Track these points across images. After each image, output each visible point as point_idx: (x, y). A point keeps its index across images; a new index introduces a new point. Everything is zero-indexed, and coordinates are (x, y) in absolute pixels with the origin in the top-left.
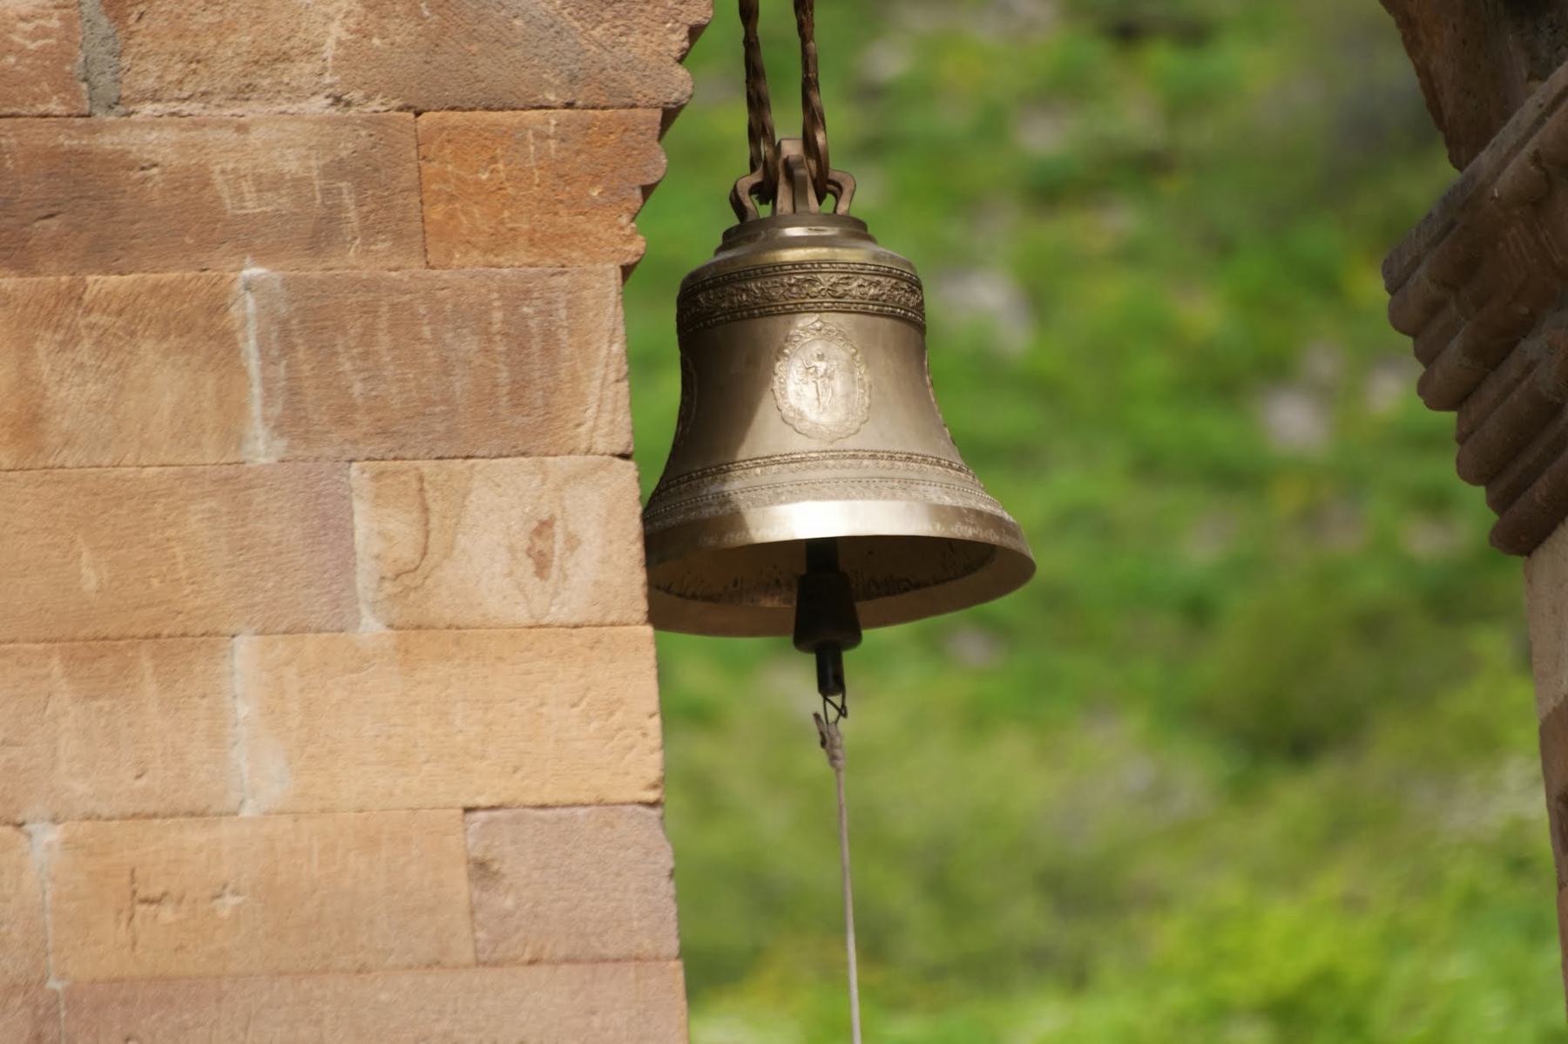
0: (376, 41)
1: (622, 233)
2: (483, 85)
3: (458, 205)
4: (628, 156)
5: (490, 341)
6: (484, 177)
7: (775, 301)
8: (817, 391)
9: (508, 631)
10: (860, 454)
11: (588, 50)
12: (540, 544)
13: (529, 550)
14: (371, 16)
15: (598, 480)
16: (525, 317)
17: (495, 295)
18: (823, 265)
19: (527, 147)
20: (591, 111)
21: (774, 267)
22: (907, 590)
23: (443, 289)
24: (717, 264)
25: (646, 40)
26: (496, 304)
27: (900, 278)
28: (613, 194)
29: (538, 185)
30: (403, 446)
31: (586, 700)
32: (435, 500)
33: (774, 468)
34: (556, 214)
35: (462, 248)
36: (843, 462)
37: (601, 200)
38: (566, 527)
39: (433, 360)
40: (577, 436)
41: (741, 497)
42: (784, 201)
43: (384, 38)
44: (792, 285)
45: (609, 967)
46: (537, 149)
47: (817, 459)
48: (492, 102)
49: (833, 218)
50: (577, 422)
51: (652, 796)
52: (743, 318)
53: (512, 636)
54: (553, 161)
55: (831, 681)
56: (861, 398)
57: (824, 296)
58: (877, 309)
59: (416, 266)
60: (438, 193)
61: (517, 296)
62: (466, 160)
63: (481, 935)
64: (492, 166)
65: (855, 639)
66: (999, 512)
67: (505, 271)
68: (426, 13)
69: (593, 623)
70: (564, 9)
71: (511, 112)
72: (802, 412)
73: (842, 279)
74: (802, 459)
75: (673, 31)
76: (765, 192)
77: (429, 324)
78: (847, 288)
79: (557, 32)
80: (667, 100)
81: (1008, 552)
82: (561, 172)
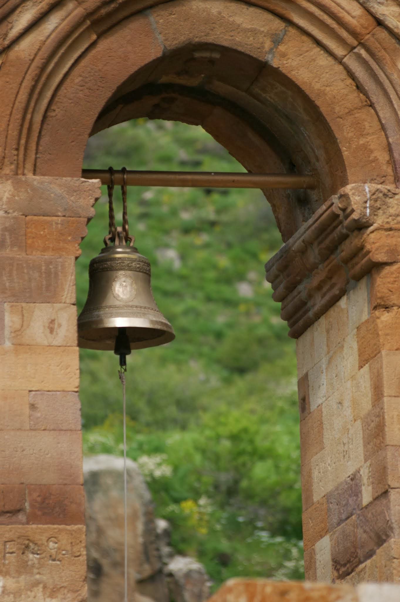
0: (16, 198)
12: (51, 325)
16: (50, 269)
33: (111, 309)
36: (128, 308)
41: (102, 315)
44: (118, 263)
51: (76, 390)
56: (134, 292)
59: (24, 255)
61: (48, 263)
65: (129, 353)
74: (118, 307)
75: (91, 199)
76: (112, 240)
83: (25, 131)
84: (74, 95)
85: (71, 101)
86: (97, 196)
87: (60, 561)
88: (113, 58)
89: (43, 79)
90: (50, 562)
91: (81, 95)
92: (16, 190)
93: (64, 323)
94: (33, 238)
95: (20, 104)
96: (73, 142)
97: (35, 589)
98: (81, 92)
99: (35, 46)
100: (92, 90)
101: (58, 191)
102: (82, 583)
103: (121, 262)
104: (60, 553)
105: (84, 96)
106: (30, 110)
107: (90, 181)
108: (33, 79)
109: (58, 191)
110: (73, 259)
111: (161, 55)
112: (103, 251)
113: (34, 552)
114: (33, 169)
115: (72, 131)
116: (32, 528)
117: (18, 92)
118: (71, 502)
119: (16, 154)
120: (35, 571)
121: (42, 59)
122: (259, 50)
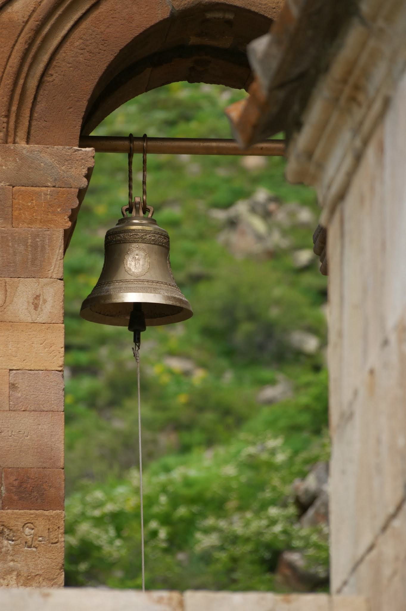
0: (4, 167)
1: (65, 221)
2: (31, 180)
3: (22, 211)
4: (69, 201)
5: (27, 247)
6: (29, 204)
7: (127, 239)
8: (135, 264)
9: (25, 323)
10: (144, 281)
11: (60, 172)
12: (36, 301)
13: (33, 302)
14: (3, 161)
15: (53, 285)
16: (37, 241)
17: (30, 235)
18: (130, 231)
19: (42, 197)
20: (59, 188)
21: (127, 230)
22: (164, 316)
23: (16, 233)
24: (117, 228)
25: (76, 170)
26: (30, 238)
27: (161, 235)
28: (63, 210)
29: (44, 207)
30: (2, 274)
31: (44, 343)
32: (9, 288)
33: (121, 283)
34: (48, 215)
35: (22, 223)
36: (139, 282)
37: (60, 212)
38: (43, 297)
39: (11, 252)
40: (48, 273)
41: (112, 290)
42: (134, 213)
43: (6, 167)
44: (131, 235)
45: (45, 413)
46: (44, 198)
47: (132, 281)
48: (33, 185)
49: (146, 219)
50: (49, 270)
51: (60, 369)
52: (118, 243)
53: (26, 325)
54: (48, 201)
55: (137, 340)
56: (147, 266)
57: (139, 239)
58: (154, 243)
59: (9, 227)
60: (16, 208)
61: (35, 236)
62: (25, 199)
63: (11, 403)
64: (32, 202)
65: (144, 329)
66: (181, 298)
67: (33, 229)
68: (18, 161)
69: (48, 323)
70: (55, 161)
71: (38, 188)
72: (131, 269)
73: (144, 234)
74: (129, 281)
75: (83, 168)
76: (130, 210)
77: (11, 242)
78: (146, 237)
79: (52, 167)
80: (80, 186)
81: (186, 309)
82: (50, 204)
83: (17, 97)
84: (74, 59)
85: (70, 65)
86: (90, 166)
87: (36, 548)
88: (117, 19)
89: (38, 42)
90: (26, 548)
91: (81, 58)
92: (3, 159)
93: (50, 299)
94: (20, 209)
95: (12, 68)
96: (70, 108)
97: (9, 577)
98: (82, 56)
99: (29, 7)
100: (93, 53)
101: (49, 160)
102: (58, 571)
103: (135, 234)
104: (36, 539)
105: (84, 60)
106: (23, 75)
107: (83, 149)
108: (26, 42)
109: (49, 160)
110: (61, 231)
111: (168, 16)
112: (121, 221)
113: (9, 538)
114: (26, 136)
115: (70, 96)
116: (7, 513)
117: (10, 56)
118: (50, 487)
119: (5, 121)
120: (9, 558)
121: (37, 21)
122: (274, 10)
